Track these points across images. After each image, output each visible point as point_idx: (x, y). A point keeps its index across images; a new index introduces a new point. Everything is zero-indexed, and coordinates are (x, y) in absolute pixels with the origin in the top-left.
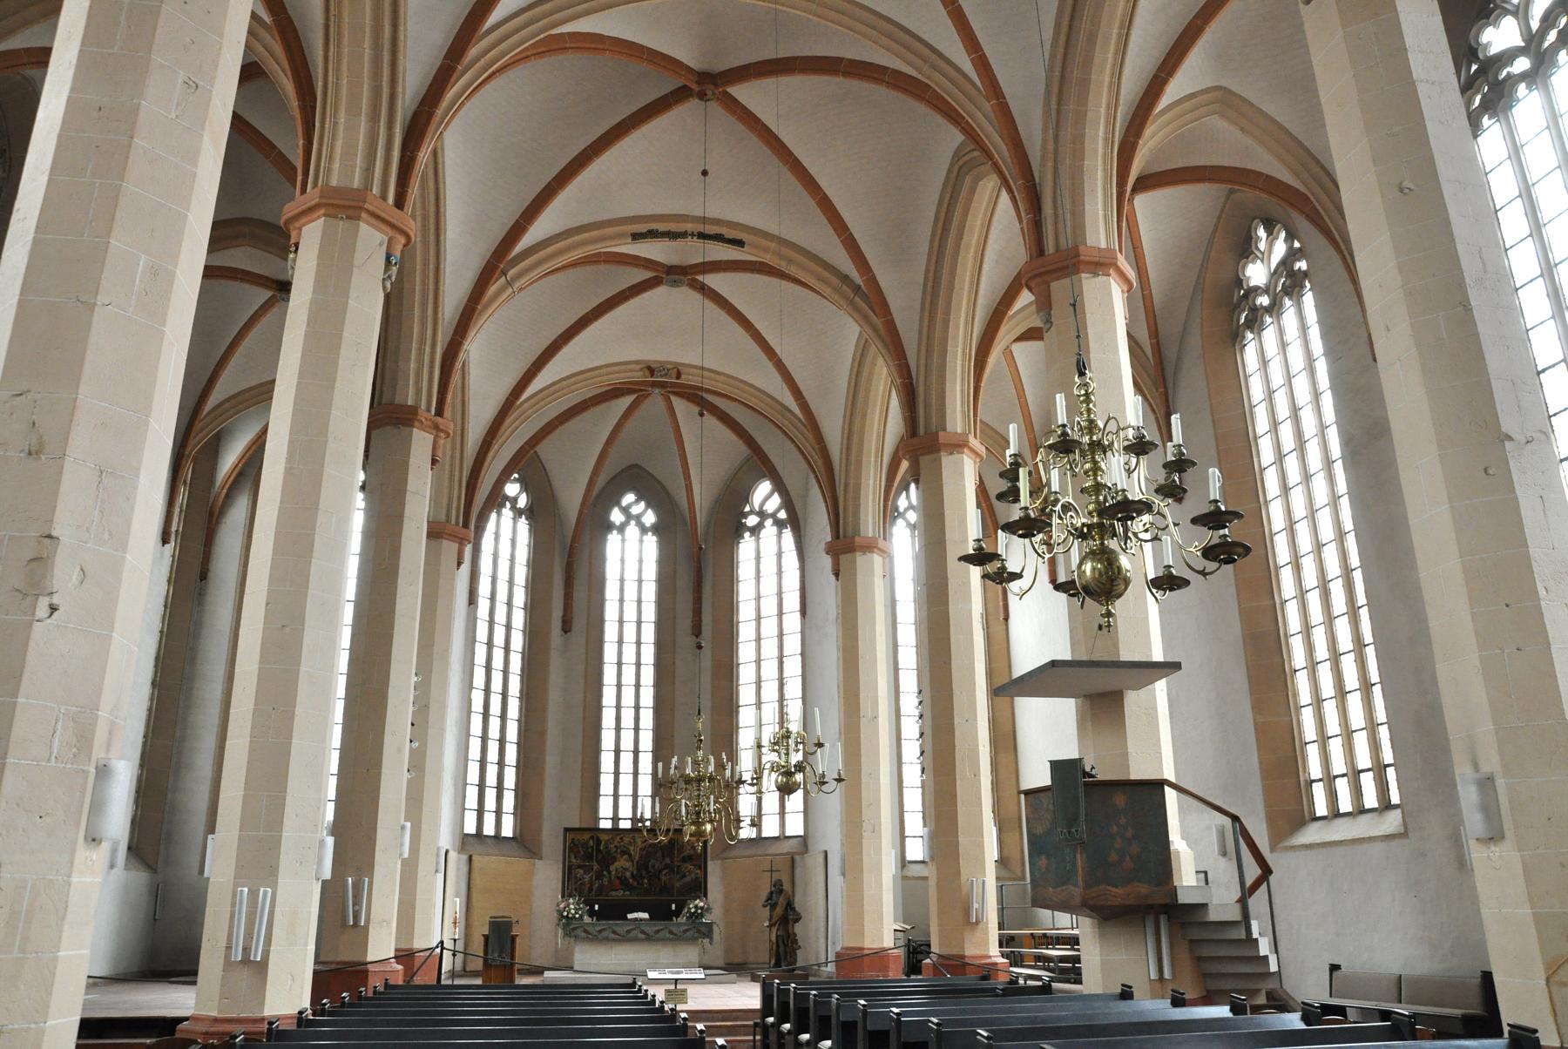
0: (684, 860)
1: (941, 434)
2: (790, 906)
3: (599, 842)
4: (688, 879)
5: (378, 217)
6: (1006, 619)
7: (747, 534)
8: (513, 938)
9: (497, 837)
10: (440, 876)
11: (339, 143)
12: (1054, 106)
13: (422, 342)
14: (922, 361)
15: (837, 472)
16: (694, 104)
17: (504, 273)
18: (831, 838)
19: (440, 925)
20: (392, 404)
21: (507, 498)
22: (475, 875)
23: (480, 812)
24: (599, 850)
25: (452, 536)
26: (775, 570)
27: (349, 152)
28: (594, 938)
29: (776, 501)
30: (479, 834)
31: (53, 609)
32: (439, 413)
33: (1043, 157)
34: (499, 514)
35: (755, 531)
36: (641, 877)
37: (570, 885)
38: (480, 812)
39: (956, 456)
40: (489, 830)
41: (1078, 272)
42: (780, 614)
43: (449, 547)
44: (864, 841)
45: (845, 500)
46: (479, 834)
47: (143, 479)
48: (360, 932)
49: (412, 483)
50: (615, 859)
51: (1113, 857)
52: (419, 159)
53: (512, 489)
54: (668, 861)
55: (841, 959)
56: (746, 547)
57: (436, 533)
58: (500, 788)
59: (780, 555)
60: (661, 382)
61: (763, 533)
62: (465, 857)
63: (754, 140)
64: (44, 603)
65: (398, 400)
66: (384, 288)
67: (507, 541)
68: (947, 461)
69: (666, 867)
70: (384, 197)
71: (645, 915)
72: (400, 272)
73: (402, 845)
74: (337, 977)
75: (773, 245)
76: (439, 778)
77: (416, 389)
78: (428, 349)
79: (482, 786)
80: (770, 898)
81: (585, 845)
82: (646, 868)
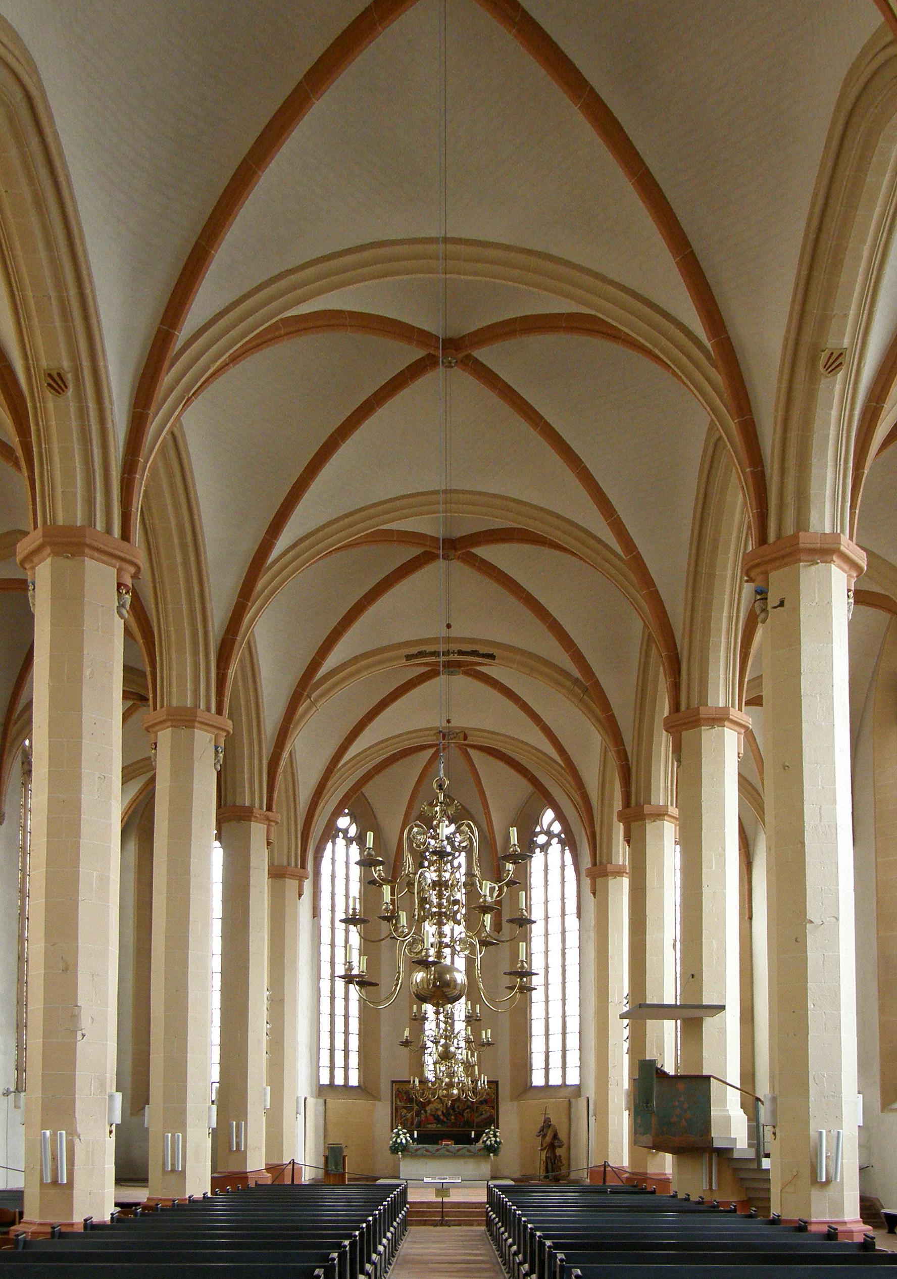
2: (555, 1136)
4: (483, 1117)
5: (206, 724)
6: (751, 918)
7: (538, 850)
8: (344, 1158)
9: (346, 1086)
10: (301, 1117)
11: (174, 673)
13: (251, 758)
14: (635, 752)
15: (595, 813)
16: (441, 563)
17: (309, 697)
18: (590, 1091)
20: (234, 806)
22: (329, 1111)
23: (332, 1068)
25: (293, 876)
28: (415, 1155)
29: (557, 828)
30: (332, 1085)
31: (83, 1035)
32: (269, 808)
33: (683, 634)
34: (334, 843)
35: (544, 848)
36: (450, 1115)
37: (397, 1118)
38: (332, 1068)
39: (658, 822)
41: (699, 726)
42: (563, 915)
43: (291, 884)
46: (332, 1085)
48: (242, 1155)
49: (254, 861)
51: (675, 1119)
52: (229, 674)
53: (343, 822)
55: (592, 1172)
56: (537, 859)
57: (277, 873)
58: (346, 1051)
59: (563, 867)
60: (454, 741)
61: (550, 849)
62: (321, 1101)
63: (494, 587)
64: (79, 1033)
65: (239, 802)
66: (216, 769)
67: (341, 867)
68: (650, 827)
70: (109, 530)
72: (225, 756)
73: (265, 1101)
74: (229, 1180)
75: (518, 657)
76: (295, 1049)
77: (251, 793)
78: (256, 762)
80: (542, 1130)
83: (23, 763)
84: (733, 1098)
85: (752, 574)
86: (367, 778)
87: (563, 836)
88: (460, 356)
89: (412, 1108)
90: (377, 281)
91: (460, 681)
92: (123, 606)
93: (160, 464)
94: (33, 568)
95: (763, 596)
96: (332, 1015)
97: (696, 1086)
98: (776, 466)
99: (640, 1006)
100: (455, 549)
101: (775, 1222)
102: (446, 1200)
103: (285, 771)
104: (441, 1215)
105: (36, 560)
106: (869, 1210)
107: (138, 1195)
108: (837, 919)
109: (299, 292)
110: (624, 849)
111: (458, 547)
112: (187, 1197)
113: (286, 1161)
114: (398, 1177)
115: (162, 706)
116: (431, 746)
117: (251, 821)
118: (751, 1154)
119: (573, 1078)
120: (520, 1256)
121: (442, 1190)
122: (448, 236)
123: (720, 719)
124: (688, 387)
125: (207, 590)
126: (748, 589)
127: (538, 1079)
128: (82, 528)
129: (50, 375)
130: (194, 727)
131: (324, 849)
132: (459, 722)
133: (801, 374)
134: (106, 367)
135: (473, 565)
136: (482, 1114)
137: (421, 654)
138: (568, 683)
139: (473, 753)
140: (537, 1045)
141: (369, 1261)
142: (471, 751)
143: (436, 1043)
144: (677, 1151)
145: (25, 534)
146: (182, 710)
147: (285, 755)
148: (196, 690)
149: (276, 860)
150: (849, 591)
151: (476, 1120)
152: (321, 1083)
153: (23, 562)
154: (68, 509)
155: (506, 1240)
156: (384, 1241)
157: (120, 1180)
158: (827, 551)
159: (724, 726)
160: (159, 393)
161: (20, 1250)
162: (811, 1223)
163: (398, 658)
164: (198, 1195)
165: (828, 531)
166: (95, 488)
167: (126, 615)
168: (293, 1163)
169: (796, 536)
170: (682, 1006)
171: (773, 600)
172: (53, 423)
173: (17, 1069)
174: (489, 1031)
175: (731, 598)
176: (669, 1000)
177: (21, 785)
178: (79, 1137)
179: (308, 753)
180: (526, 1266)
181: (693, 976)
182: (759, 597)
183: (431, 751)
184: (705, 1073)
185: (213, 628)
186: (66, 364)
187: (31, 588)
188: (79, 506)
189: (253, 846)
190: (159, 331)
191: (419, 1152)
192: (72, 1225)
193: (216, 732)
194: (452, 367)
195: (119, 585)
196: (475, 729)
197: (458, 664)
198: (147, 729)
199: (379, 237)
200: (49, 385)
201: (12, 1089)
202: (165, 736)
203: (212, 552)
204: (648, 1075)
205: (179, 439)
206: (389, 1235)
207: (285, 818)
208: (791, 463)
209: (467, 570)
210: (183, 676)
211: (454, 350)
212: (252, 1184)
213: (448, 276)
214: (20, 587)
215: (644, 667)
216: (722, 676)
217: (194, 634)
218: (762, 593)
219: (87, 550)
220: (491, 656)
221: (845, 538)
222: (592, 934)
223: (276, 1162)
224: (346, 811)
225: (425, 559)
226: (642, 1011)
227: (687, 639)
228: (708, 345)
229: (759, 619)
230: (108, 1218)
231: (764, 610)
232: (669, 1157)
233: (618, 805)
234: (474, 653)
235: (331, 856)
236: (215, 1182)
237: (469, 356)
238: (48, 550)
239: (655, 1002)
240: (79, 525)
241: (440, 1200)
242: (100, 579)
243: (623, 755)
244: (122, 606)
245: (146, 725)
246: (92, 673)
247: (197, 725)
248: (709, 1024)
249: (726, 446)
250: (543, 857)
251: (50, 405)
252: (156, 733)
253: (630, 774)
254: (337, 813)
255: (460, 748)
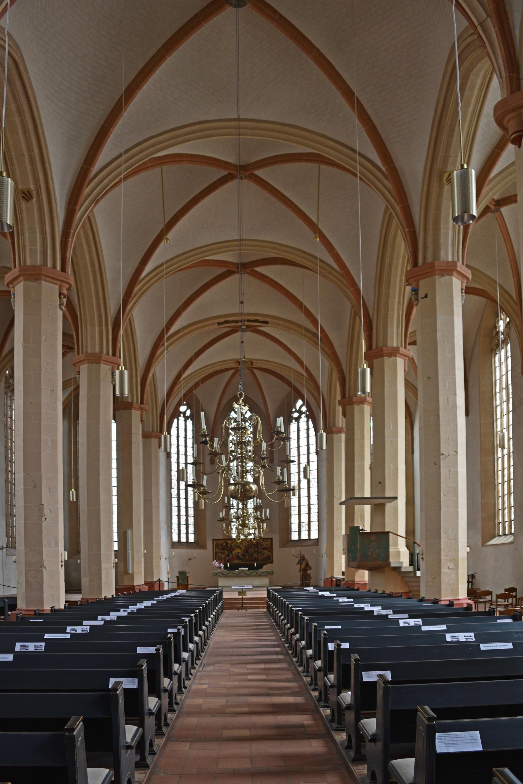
0: (263, 549)
1: (384, 348)
2: (307, 564)
3: (227, 543)
4: (264, 556)
5: (107, 361)
7: (294, 421)
8: (187, 577)
12: (377, 290)
14: (348, 369)
16: (236, 181)
19: (164, 573)
20: (122, 402)
21: (181, 413)
24: (227, 547)
25: (155, 437)
26: (306, 436)
27: (93, 338)
28: (225, 576)
29: (304, 409)
31: (46, 519)
32: (142, 403)
35: (298, 419)
40: (184, 539)
43: (154, 441)
44: (335, 542)
45: (329, 413)
47: (59, 488)
50: (234, 549)
51: (370, 553)
54: (256, 549)
57: (146, 436)
59: (308, 429)
61: (301, 420)
64: (43, 518)
68: (356, 408)
69: (256, 551)
71: (247, 569)
76: (158, 524)
78: (134, 379)
79: (179, 524)
81: (222, 545)
82: (247, 552)
83: (5, 383)
84: (402, 542)
85: (410, 281)
86: (197, 385)
87: (308, 413)
88: (247, 173)
89: (224, 553)
90: (201, 140)
91: (249, 335)
92: (62, 304)
93: (82, 234)
94: (14, 287)
95: (416, 292)
96: (179, 507)
97: (381, 538)
98: (422, 228)
99: (351, 498)
100: (246, 268)
101: (422, 600)
102: (244, 597)
103: (150, 383)
104: (241, 604)
105: (15, 283)
106: (472, 593)
107: (76, 597)
108: (457, 452)
109: (159, 146)
110: (342, 419)
111: (246, 267)
112: (103, 597)
113: (155, 580)
114: (218, 587)
115: (82, 353)
116: (232, 369)
117: (131, 409)
118: (411, 569)
119: (314, 535)
120: (286, 621)
121: (242, 592)
122: (240, 117)
123: (394, 352)
124: (372, 188)
125: (106, 294)
126: (408, 288)
127: (295, 536)
128: (40, 266)
129: (24, 193)
130: (100, 363)
131: (173, 423)
132: (249, 356)
133: (435, 184)
134: (54, 187)
135: (255, 276)
136: (263, 555)
137: (227, 322)
138: (310, 335)
139: (257, 372)
140: (294, 520)
141: (204, 625)
142: (255, 371)
143: (238, 518)
144: (369, 569)
145: (10, 269)
146: (93, 355)
147: (150, 375)
148: (101, 344)
149: (146, 428)
150: (462, 289)
151: (260, 558)
152: (174, 541)
153: (8, 285)
154: (32, 258)
155: (278, 614)
156: (212, 616)
157: (69, 590)
158: (450, 269)
159: (396, 356)
160: (82, 199)
161: (19, 621)
162: (441, 601)
163: (214, 324)
164: (109, 596)
165: (450, 259)
166: (47, 246)
167: (64, 309)
168: (159, 580)
169: (433, 263)
170: (371, 498)
171: (421, 294)
172: (25, 215)
173: (7, 536)
174: (268, 510)
175: (399, 293)
176: (367, 494)
177: (4, 393)
178: (45, 568)
179: (163, 375)
180: (289, 625)
181: (380, 483)
182: (414, 293)
183: (232, 371)
184: (387, 530)
185: (110, 312)
186: (32, 187)
187: (12, 296)
188: (38, 257)
189: (133, 423)
190: (82, 168)
191: (229, 574)
192: (43, 610)
193: (112, 365)
194: (242, 179)
195: (60, 294)
196: (257, 360)
197: (248, 327)
198: (74, 365)
199: (202, 119)
200: (23, 197)
201: (5, 546)
202: (84, 368)
203: (109, 276)
204: (354, 533)
205: (92, 220)
206: (214, 613)
207: (150, 407)
208: (430, 227)
209: (253, 279)
210: (93, 338)
211: (244, 171)
212: (137, 591)
213: (241, 137)
214: (7, 295)
215: (352, 327)
216: (395, 331)
217: (100, 316)
218: (415, 291)
219: (43, 277)
220: (266, 322)
221: (459, 264)
222: (325, 463)
223: (150, 580)
224: (185, 403)
225: (228, 273)
226: (352, 501)
227: (375, 313)
228: (384, 169)
229: (415, 304)
230: (62, 607)
231: (417, 299)
232: (367, 572)
233: (338, 397)
234: (256, 321)
235: (176, 426)
236: (117, 590)
237: (252, 174)
238: (22, 278)
239: (360, 496)
240: (38, 265)
241: (241, 597)
242: (49, 291)
243: (341, 371)
244: (61, 304)
245: (74, 362)
246: (46, 338)
247: (102, 361)
248: (389, 506)
249: (394, 218)
250: (296, 425)
251: (23, 207)
252: (79, 366)
253: (345, 380)
254: (180, 404)
255: (249, 369)
